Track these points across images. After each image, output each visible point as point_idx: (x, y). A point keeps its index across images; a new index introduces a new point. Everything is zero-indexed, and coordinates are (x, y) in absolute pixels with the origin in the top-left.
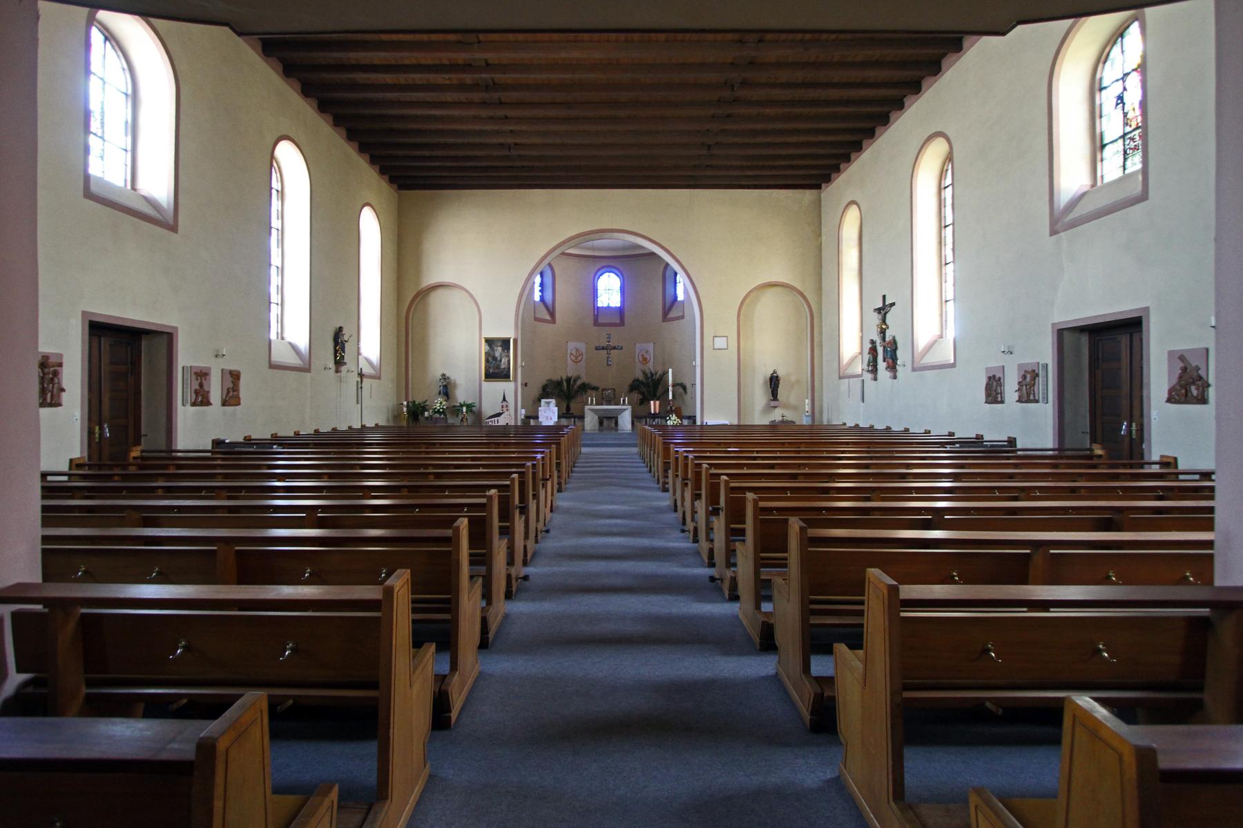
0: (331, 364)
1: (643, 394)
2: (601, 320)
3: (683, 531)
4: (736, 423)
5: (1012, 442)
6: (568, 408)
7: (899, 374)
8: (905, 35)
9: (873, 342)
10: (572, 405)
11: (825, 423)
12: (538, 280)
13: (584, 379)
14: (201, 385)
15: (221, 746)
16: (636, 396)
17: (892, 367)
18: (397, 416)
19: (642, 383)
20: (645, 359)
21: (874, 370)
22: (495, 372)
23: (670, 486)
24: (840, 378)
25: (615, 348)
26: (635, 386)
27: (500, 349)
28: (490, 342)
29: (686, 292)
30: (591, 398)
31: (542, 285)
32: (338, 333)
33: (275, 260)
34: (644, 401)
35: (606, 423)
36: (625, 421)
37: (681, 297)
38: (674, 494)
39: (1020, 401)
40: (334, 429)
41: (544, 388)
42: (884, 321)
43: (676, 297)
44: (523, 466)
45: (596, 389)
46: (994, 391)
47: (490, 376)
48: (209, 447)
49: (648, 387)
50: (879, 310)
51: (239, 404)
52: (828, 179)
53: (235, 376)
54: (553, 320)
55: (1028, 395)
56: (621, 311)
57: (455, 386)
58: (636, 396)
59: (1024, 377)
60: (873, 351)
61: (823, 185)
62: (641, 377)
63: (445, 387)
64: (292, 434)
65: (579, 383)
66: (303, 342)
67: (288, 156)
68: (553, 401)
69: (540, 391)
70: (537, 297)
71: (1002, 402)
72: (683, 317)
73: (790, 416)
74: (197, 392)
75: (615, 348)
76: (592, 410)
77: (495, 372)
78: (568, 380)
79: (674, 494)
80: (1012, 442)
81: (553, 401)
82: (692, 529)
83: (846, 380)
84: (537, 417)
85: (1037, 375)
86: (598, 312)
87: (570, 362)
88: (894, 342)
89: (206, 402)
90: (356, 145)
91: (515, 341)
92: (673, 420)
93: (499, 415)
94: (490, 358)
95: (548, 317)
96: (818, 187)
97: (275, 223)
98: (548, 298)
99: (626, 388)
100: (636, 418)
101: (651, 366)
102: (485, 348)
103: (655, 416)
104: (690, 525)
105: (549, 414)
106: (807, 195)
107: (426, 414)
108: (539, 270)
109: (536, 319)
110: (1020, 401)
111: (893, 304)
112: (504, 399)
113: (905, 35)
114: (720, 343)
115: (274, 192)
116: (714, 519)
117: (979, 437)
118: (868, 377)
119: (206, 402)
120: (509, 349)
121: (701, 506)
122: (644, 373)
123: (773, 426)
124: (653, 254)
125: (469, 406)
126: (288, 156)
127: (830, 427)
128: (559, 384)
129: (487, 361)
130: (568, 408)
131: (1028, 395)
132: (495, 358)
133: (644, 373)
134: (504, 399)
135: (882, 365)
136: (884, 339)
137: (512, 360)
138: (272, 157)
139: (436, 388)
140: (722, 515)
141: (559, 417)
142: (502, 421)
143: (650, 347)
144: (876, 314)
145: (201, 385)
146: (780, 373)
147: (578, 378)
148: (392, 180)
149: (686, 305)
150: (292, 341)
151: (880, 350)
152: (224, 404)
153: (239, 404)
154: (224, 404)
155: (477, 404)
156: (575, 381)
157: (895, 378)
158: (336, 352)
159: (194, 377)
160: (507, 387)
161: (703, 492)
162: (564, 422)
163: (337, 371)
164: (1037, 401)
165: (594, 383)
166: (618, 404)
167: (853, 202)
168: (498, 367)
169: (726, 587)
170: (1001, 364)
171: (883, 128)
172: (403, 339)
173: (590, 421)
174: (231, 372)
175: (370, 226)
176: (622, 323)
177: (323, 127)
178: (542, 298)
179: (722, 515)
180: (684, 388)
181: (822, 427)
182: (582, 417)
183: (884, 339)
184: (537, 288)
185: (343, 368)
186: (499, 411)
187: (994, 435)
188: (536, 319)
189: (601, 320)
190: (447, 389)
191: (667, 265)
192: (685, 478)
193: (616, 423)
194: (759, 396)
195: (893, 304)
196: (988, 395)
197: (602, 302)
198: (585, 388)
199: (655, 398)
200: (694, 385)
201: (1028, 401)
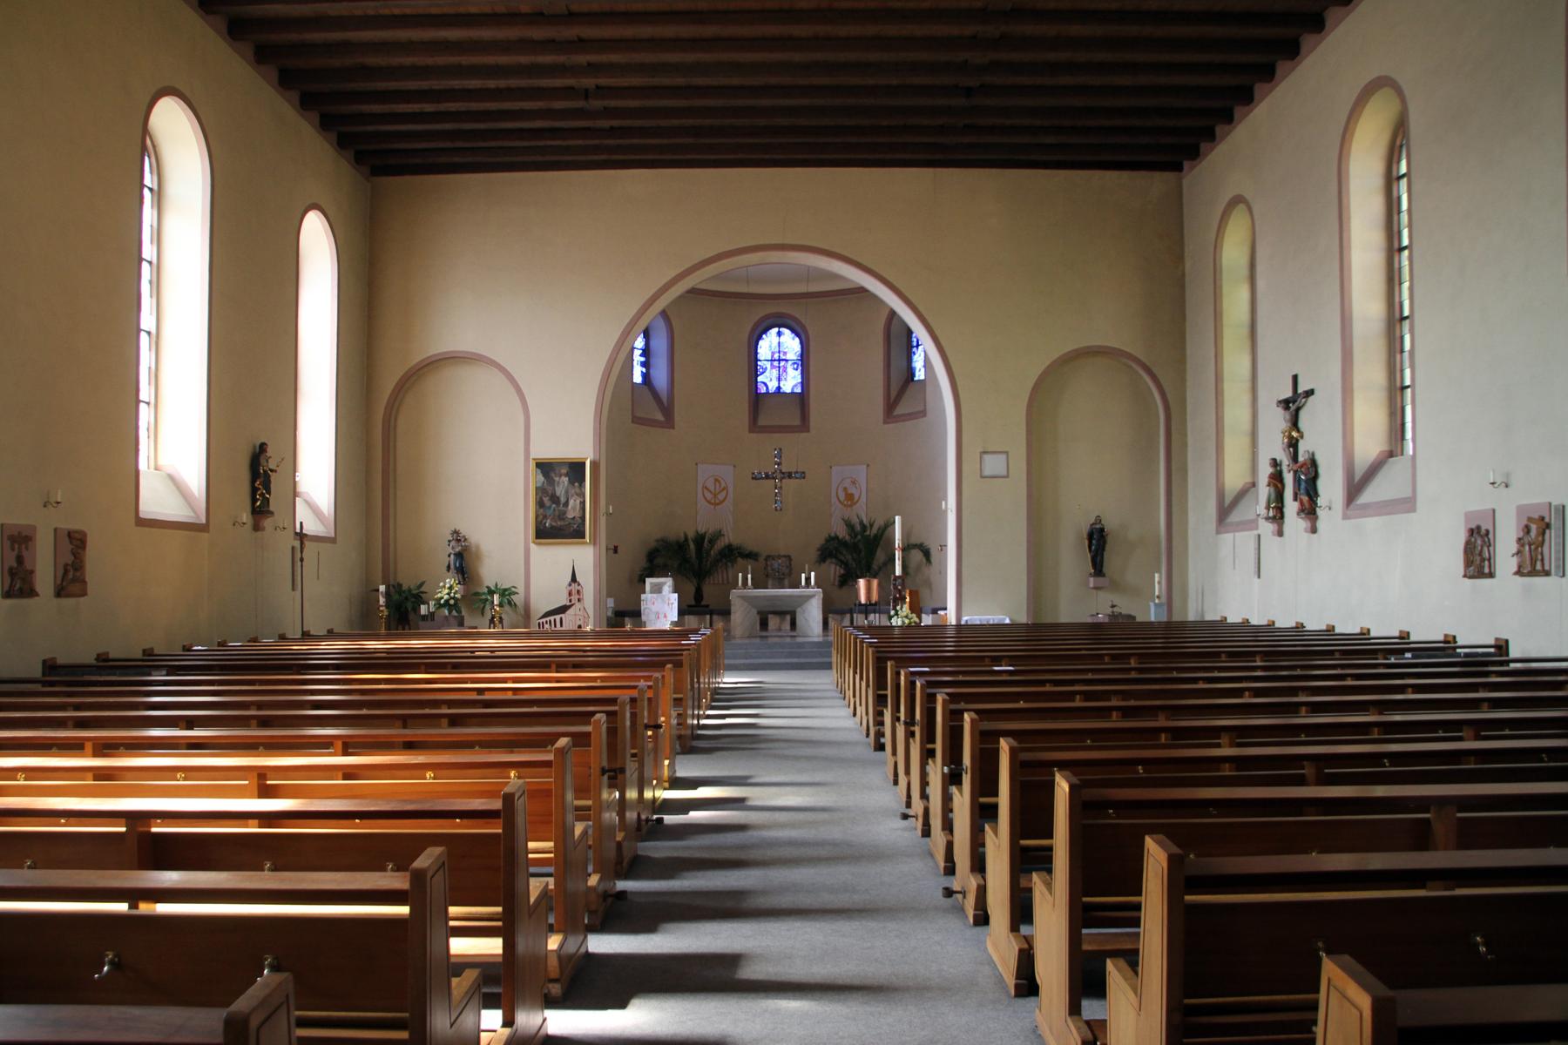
0: (246, 517)
1: (844, 564)
3: (905, 817)
4: (1023, 618)
5: (1502, 647)
6: (699, 595)
7: (1320, 524)
9: (1275, 463)
10: (708, 589)
11: (1191, 617)
12: (640, 343)
13: (731, 537)
14: (20, 559)
15: (254, 1022)
16: (833, 570)
17: (1310, 511)
19: (843, 543)
20: (850, 497)
21: (1278, 516)
22: (553, 527)
23: (887, 740)
25: (790, 475)
26: (830, 550)
27: (565, 480)
28: (545, 467)
29: (927, 364)
30: (744, 576)
31: (646, 352)
32: (258, 455)
33: (147, 321)
34: (848, 580)
35: (773, 622)
36: (812, 615)
37: (920, 375)
38: (894, 753)
39: (1519, 573)
40: (1300, 626)
41: (652, 555)
42: (1295, 423)
44: (613, 701)
45: (751, 556)
46: (1478, 562)
47: (544, 533)
48: (37, 672)
49: (856, 552)
50: (1286, 404)
51: (84, 594)
52: (1194, 154)
53: (77, 541)
54: (669, 422)
55: (1533, 562)
57: (478, 556)
58: (833, 570)
59: (1527, 530)
60: (1277, 478)
61: (1186, 164)
62: (842, 532)
63: (459, 555)
64: (139, 655)
65: (720, 544)
66: (194, 476)
67: (176, 133)
68: (668, 583)
69: (643, 563)
70: (638, 379)
71: (1491, 575)
72: (923, 413)
73: (1126, 606)
74: (12, 573)
75: (790, 475)
76: (743, 598)
77: (553, 527)
78: (700, 539)
79: (894, 753)
80: (1502, 647)
81: (668, 583)
82: (920, 812)
84: (636, 614)
85: (1548, 526)
86: (758, 400)
87: (702, 503)
88: (1313, 463)
89: (28, 591)
90: (295, 95)
91: (595, 465)
93: (563, 610)
95: (660, 417)
96: (1178, 167)
97: (148, 251)
98: (660, 378)
99: (813, 554)
100: (828, 609)
101: (861, 512)
103: (867, 609)
104: (918, 806)
105: (662, 606)
106: (1157, 182)
107: (423, 609)
108: (643, 324)
109: (637, 420)
110: (1519, 573)
111: (1310, 393)
112: (574, 579)
115: (146, 192)
116: (954, 789)
117: (1450, 640)
118: (1267, 528)
119: (28, 591)
121: (936, 771)
122: (849, 525)
123: (1094, 631)
124: (862, 290)
125: (506, 593)
126: (176, 133)
127: (1220, 627)
128: (679, 548)
129: (540, 504)
130: (699, 595)
131: (1533, 563)
132: (555, 499)
133: (849, 525)
134: (574, 579)
135: (1291, 507)
136: (1295, 458)
137: (585, 501)
138: (145, 130)
139: (443, 554)
140: (966, 780)
141: (681, 613)
142: (569, 621)
143: (861, 473)
144: (1280, 411)
145: (20, 559)
146: (1110, 524)
147: (719, 534)
148: (360, 159)
149: (929, 389)
150: (171, 471)
151: (1289, 478)
152: (60, 592)
153: (84, 594)
154: (60, 592)
155: (521, 590)
156: (712, 541)
157: (1314, 530)
158: (254, 490)
159: (7, 544)
160: (582, 558)
161: (939, 746)
162: (691, 621)
163: (257, 527)
164: (1547, 574)
165: (750, 546)
166: (797, 585)
167: (1238, 200)
168: (562, 516)
169: (970, 904)
170: (1489, 506)
171: (1288, 64)
173: (741, 616)
174: (70, 534)
175: (316, 241)
177: (232, 65)
178: (645, 376)
179: (966, 780)
180: (927, 554)
181: (1183, 626)
182: (726, 613)
183: (1295, 458)
184: (638, 358)
185: (268, 523)
186: (565, 602)
187: (1474, 634)
190: (464, 562)
191: (893, 314)
192: (910, 722)
193: (793, 624)
194: (1071, 561)
195: (1310, 393)
196: (1468, 563)
197: (768, 380)
198: (733, 554)
199: (868, 571)
200: (943, 547)
201: (1533, 573)
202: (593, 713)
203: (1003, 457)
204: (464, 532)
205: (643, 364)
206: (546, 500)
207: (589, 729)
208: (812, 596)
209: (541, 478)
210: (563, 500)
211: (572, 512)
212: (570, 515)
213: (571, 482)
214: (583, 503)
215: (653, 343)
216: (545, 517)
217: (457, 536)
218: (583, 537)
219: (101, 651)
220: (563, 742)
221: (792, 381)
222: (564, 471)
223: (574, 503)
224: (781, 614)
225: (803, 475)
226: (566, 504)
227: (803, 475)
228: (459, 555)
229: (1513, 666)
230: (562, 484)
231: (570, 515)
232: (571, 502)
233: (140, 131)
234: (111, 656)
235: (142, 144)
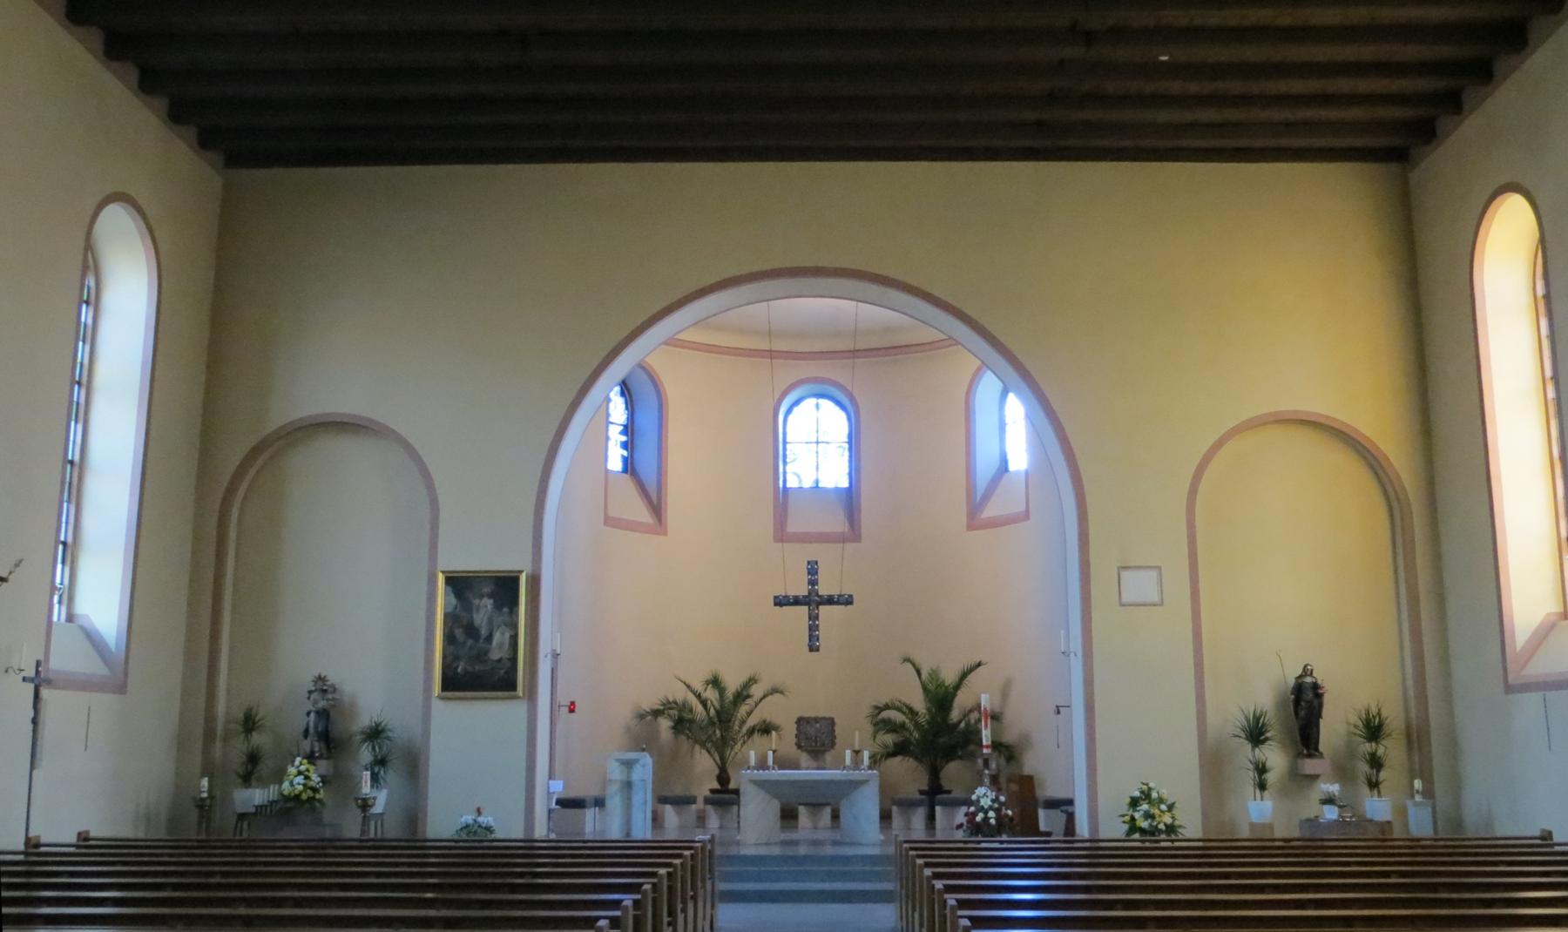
2: (793, 527)
8: (1400, 551)
18: (174, 820)
24: (1509, 689)
25: (830, 601)
27: (488, 603)
28: (460, 584)
31: (628, 429)
43: (1003, 467)
47: (455, 683)
56: (850, 499)
63: (323, 714)
70: (615, 461)
75: (830, 601)
76: (761, 784)
83: (1534, 698)
86: (783, 498)
90: (162, 103)
92: (1002, 798)
94: (460, 630)
95: (643, 514)
102: (442, 599)
109: (609, 521)
113: (1400, 551)
114: (1140, 586)
120: (514, 602)
129: (449, 638)
132: (471, 631)
148: (207, 141)
168: (482, 656)
172: (209, 575)
176: (853, 533)
178: (629, 466)
184: (616, 436)
188: (609, 521)
189: (793, 527)
193: (835, 816)
202: (598, 918)
203: (1126, 598)
204: (333, 678)
205: (625, 445)
206: (459, 633)
207: (618, 913)
208: (855, 785)
209: (453, 600)
210: (484, 632)
211: (497, 651)
212: (495, 655)
213: (498, 607)
214: (514, 638)
215: (638, 418)
216: (457, 658)
217: (322, 686)
218: (972, 834)
219: (82, 829)
220: (602, 923)
221: (836, 475)
222: (486, 590)
223: (500, 637)
224: (815, 806)
225: (848, 601)
226: (489, 638)
227: (848, 601)
228: (323, 714)
230: (484, 610)
231: (495, 655)
232: (497, 637)
233: (82, 244)
234: (43, 840)
235: (89, 263)
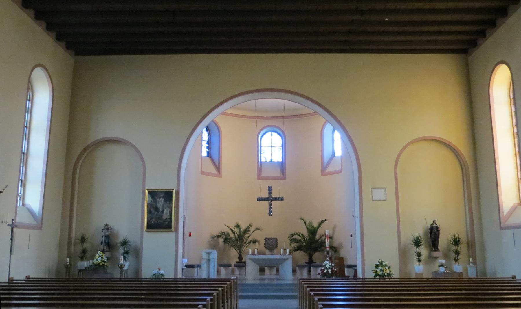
27: (162, 200)
28: (153, 194)
31: (209, 142)
47: (151, 226)
70: (204, 153)
76: (253, 260)
90: (54, 34)
95: (214, 171)
109: (202, 173)
132: (157, 209)
148: (69, 47)
168: (160, 218)
178: (209, 154)
184: (205, 145)
193: (278, 271)
202: (199, 305)
203: (374, 198)
204: (111, 225)
205: (208, 148)
206: (152, 210)
207: (205, 303)
209: (151, 199)
210: (161, 210)
211: (165, 216)
212: (164, 217)
213: (165, 201)
214: (171, 212)
215: (212, 138)
216: (152, 218)
217: (107, 227)
219: (27, 275)
220: (200, 306)
221: (278, 157)
222: (162, 196)
223: (166, 211)
224: (271, 267)
225: (282, 199)
226: (163, 212)
227: (282, 199)
228: (107, 237)
229: (518, 281)
230: (161, 202)
231: (164, 217)
232: (165, 211)
234: (14, 278)
